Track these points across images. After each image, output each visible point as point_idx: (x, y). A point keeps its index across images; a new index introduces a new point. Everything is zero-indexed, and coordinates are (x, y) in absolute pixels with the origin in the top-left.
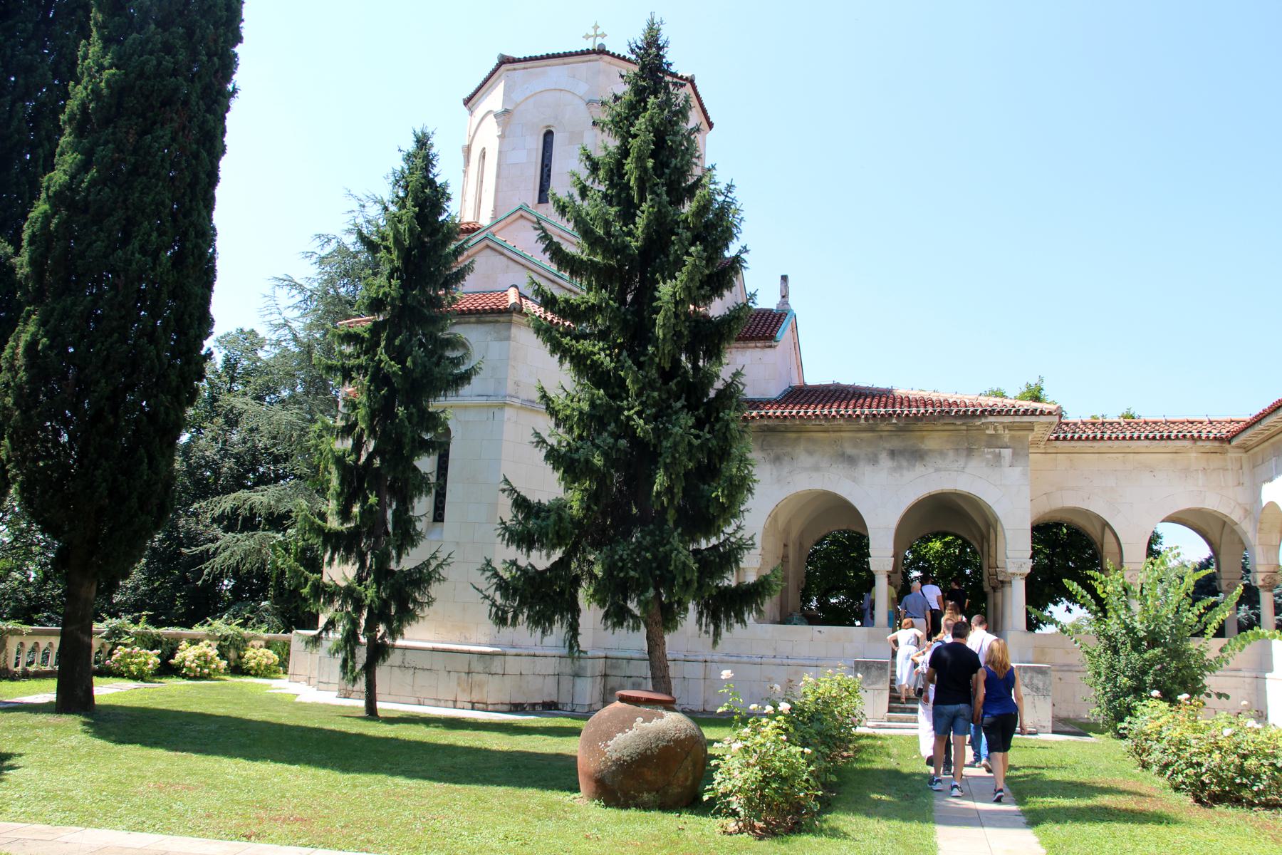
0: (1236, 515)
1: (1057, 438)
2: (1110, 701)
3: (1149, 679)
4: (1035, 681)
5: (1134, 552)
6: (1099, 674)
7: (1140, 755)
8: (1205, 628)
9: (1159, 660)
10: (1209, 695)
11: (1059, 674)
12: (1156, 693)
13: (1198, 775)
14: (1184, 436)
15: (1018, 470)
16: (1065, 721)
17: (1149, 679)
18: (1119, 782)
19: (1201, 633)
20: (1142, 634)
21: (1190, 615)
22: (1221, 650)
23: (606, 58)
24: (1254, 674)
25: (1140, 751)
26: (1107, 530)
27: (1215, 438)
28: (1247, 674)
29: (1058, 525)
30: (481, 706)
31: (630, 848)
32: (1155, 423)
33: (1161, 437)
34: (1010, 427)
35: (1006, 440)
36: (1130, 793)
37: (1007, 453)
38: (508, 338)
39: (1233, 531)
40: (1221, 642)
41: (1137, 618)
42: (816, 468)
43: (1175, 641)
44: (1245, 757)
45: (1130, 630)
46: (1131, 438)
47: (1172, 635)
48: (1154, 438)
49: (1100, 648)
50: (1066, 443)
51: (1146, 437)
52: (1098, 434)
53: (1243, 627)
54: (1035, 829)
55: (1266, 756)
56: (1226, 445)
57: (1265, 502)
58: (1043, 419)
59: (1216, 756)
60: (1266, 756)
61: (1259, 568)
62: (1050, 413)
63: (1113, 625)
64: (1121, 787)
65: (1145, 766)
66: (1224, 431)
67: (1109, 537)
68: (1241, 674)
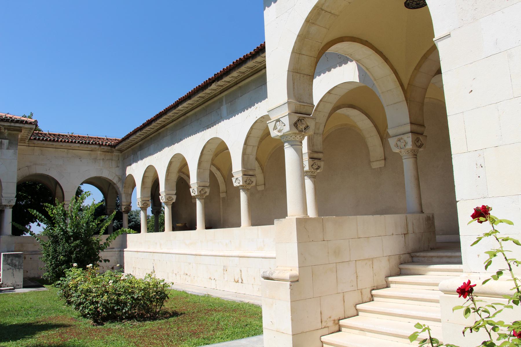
0: (115, 181)
1: (35, 139)
2: (54, 269)
3: (74, 256)
4: (14, 261)
5: (69, 195)
6: (49, 255)
7: (67, 298)
8: (100, 230)
9: (77, 246)
10: (101, 261)
11: (31, 256)
12: (75, 265)
13: (96, 308)
14: (96, 143)
15: (11, 152)
16: (33, 279)
17: (74, 256)
18: (53, 318)
19: (98, 233)
20: (71, 234)
21: (94, 224)
22: (107, 240)
24: (119, 250)
25: (67, 295)
26: (58, 186)
27: (109, 145)
28: (116, 250)
29: (35, 183)
32: (84, 137)
33: (85, 143)
34: (9, 129)
35: (6, 135)
37: (6, 142)
39: (114, 188)
40: (107, 236)
41: (69, 226)
43: (86, 237)
44: (119, 295)
45: (65, 232)
46: (72, 142)
47: (85, 233)
48: (82, 143)
49: (50, 242)
50: (39, 142)
51: (79, 142)
52: (56, 139)
53: (115, 229)
55: (129, 294)
56: (113, 149)
57: (127, 173)
58: (27, 126)
59: (105, 297)
60: (129, 294)
61: (123, 204)
62: (31, 123)
63: (57, 230)
64: (54, 322)
65: (69, 303)
66: (113, 143)
67: (58, 189)
68: (114, 250)
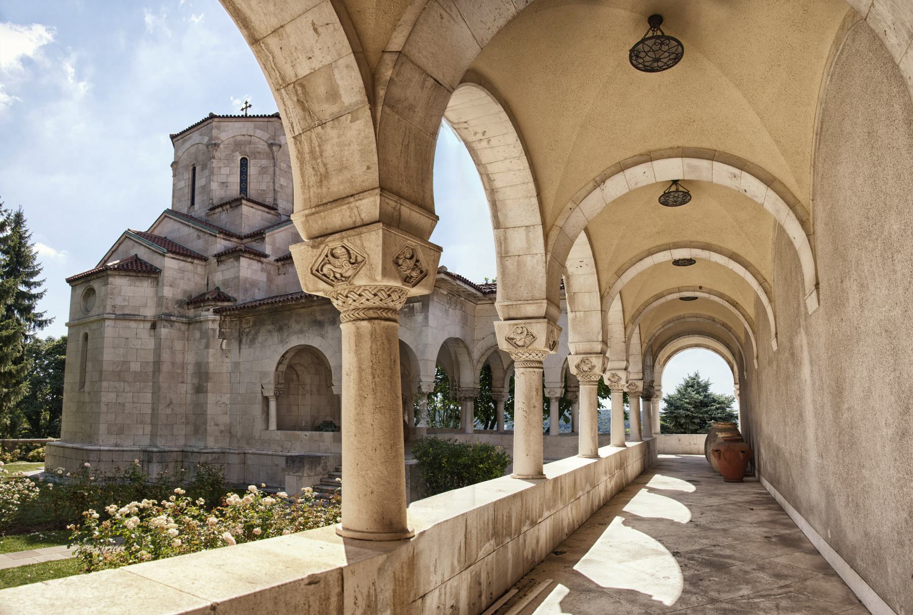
23: (216, 120)
30: (761, 279)
31: (909, 197)
36: (326, 204)
38: (107, 284)
42: (301, 332)
54: (465, 69)
